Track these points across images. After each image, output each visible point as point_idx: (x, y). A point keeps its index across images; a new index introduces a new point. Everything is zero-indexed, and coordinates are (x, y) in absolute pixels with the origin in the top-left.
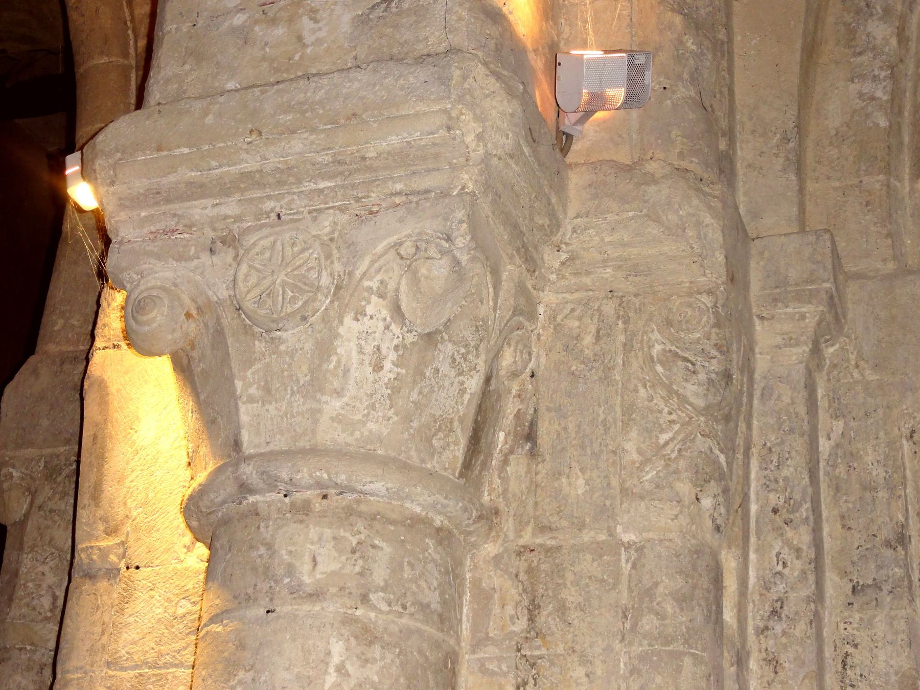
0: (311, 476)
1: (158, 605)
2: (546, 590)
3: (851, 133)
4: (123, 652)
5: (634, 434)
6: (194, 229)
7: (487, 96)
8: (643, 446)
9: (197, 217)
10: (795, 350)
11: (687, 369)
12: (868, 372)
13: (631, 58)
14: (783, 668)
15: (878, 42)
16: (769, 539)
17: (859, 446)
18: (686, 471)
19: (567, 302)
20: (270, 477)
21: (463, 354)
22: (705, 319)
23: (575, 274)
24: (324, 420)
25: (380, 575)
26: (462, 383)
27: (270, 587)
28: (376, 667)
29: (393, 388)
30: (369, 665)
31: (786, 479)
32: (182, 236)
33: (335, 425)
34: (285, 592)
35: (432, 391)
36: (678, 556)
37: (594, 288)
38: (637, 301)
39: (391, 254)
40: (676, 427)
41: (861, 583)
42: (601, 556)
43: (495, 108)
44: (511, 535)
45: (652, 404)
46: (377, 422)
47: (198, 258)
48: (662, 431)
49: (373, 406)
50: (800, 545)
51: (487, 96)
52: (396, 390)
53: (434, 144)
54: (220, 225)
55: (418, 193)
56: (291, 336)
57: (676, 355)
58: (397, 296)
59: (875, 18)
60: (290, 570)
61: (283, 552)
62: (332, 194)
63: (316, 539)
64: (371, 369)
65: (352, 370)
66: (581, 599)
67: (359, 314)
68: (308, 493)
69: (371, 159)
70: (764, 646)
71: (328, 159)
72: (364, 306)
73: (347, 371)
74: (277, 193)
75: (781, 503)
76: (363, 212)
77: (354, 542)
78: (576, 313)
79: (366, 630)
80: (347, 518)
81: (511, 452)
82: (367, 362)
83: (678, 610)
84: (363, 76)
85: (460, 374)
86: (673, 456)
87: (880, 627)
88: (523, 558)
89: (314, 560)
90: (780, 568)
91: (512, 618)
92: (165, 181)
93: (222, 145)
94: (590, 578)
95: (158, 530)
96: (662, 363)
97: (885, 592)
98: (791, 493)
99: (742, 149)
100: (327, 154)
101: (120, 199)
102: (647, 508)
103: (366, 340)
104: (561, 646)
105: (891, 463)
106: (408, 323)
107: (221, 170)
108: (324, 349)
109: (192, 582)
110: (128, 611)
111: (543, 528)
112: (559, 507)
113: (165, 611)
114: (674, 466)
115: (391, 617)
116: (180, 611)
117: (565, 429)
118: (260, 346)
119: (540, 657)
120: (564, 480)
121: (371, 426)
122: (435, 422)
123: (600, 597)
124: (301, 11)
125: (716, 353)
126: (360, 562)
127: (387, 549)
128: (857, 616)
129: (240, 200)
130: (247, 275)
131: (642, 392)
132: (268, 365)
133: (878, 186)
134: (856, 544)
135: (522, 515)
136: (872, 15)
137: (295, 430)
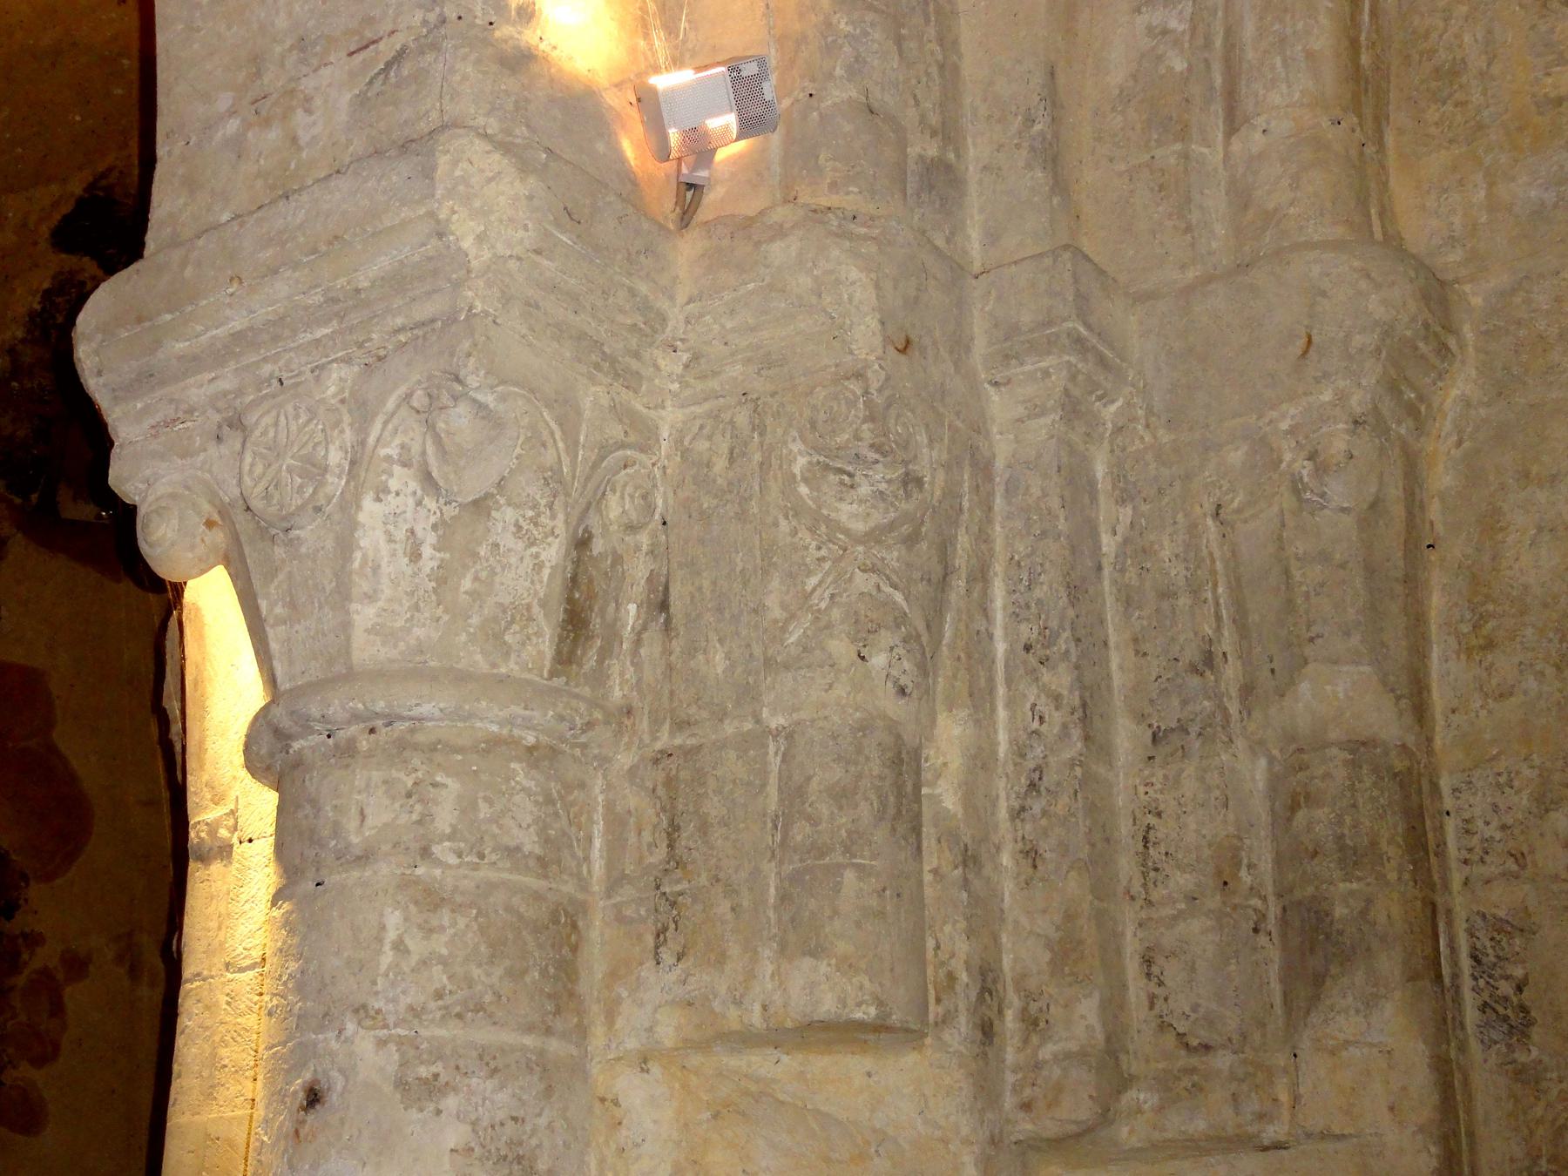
0: (344, 708)
4: (240, 949)
5: (775, 583)
7: (490, 180)
10: (1042, 421)
11: (842, 483)
12: (1161, 432)
14: (1044, 860)
16: (1021, 687)
18: (842, 622)
21: (531, 519)
24: (358, 637)
25: (445, 817)
26: (537, 556)
28: (444, 938)
30: (435, 936)
31: (1039, 602)
35: (493, 573)
36: (834, 738)
39: (404, 412)
43: (503, 193)
45: (796, 540)
46: (424, 625)
48: (809, 573)
49: (417, 608)
51: (490, 180)
53: (430, 259)
54: (220, 404)
56: (308, 532)
57: (827, 467)
60: (337, 830)
64: (406, 560)
65: (384, 564)
67: (381, 492)
70: (1020, 834)
71: (319, 298)
73: (376, 569)
75: (1034, 636)
77: (410, 784)
79: (428, 892)
81: (645, 628)
82: (400, 553)
84: (343, 184)
85: (532, 544)
86: (823, 605)
87: (1189, 786)
90: (1036, 725)
91: (650, 845)
96: (806, 480)
97: (1193, 735)
99: (975, 145)
102: (795, 680)
103: (395, 524)
104: (704, 875)
105: (1192, 554)
107: (209, 334)
108: (346, 546)
111: (681, 725)
115: (462, 871)
117: (700, 589)
118: (279, 552)
119: (681, 894)
120: (701, 657)
122: (504, 612)
124: (294, 103)
125: (877, 456)
126: (418, 807)
127: (453, 785)
128: (1160, 773)
130: (252, 465)
133: (1172, 161)
134: (1154, 675)
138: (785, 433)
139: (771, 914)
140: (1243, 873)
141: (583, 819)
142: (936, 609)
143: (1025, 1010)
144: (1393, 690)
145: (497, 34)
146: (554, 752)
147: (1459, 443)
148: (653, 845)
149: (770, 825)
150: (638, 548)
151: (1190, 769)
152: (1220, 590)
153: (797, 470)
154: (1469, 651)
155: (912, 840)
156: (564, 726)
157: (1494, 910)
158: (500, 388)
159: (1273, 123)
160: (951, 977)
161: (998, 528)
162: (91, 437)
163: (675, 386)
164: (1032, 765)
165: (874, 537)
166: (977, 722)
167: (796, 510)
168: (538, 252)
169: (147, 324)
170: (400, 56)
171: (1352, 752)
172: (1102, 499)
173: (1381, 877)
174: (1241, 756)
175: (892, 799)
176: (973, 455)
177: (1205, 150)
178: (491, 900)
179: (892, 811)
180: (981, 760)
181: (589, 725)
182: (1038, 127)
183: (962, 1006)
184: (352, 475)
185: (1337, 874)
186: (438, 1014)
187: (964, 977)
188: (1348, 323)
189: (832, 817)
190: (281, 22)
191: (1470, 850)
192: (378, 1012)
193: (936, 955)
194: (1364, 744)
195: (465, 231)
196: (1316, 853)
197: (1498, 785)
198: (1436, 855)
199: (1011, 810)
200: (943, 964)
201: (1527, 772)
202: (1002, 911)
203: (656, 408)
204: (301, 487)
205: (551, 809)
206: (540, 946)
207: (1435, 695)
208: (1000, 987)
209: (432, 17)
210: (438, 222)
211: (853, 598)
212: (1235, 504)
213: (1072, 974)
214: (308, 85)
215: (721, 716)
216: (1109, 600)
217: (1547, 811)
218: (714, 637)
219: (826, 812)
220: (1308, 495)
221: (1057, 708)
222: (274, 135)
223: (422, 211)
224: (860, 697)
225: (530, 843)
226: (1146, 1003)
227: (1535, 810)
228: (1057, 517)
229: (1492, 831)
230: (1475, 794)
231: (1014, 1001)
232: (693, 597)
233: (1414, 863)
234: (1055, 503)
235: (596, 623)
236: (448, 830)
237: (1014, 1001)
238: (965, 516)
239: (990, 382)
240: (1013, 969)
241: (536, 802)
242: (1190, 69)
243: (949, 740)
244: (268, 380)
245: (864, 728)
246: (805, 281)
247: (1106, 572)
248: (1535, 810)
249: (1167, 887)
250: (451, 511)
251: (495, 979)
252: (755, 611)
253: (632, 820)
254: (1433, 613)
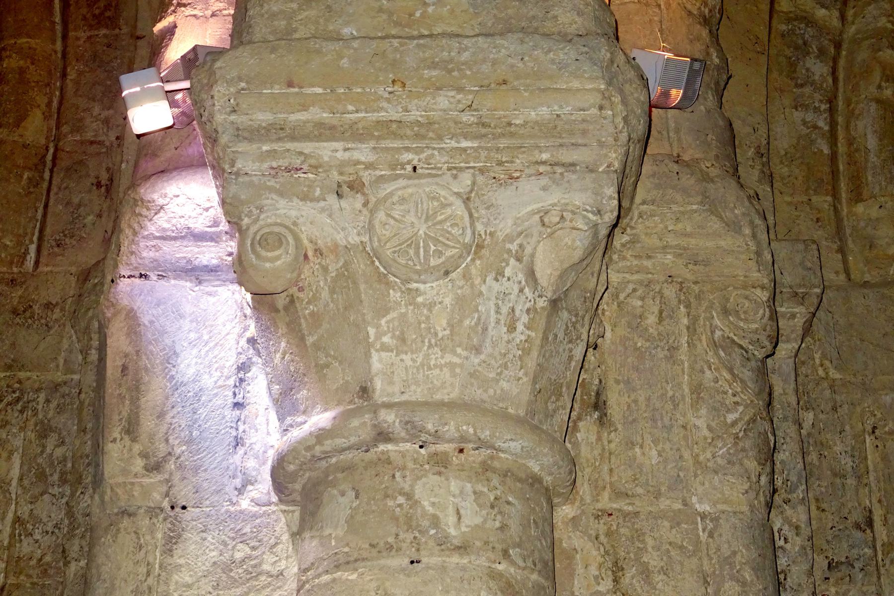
1: (212, 547)
2: (628, 553)
3: (798, 155)
5: (703, 411)
6: (320, 170)
8: (713, 424)
9: (326, 159)
15: (817, 78)
17: (828, 436)
18: (751, 449)
19: (628, 282)
20: (414, 427)
22: (761, 312)
23: (635, 256)
26: (571, 350)
27: (415, 538)
29: (523, 350)
32: (305, 176)
33: (473, 380)
34: (431, 543)
37: (653, 271)
38: (696, 288)
40: (741, 409)
41: (836, 560)
42: (678, 524)
44: (588, 499)
46: (508, 381)
47: (325, 200)
48: (729, 411)
50: (799, 523)
52: (526, 352)
55: (563, 165)
57: (733, 341)
58: (532, 261)
59: (812, 56)
60: (435, 522)
61: (426, 503)
62: (473, 154)
63: (457, 492)
64: (505, 329)
66: (662, 564)
68: (446, 445)
69: (516, 125)
72: (504, 268)
73: (485, 329)
74: (414, 146)
76: (502, 176)
77: (492, 498)
78: (638, 293)
80: (483, 474)
82: (503, 322)
83: (755, 579)
85: (570, 342)
88: (602, 522)
89: (458, 513)
91: (596, 578)
92: (293, 117)
93: (359, 90)
94: (670, 543)
95: (206, 470)
98: (788, 474)
100: (473, 115)
102: (720, 482)
103: (503, 300)
106: (539, 288)
109: (249, 526)
110: (177, 552)
111: (619, 494)
112: (634, 475)
113: (221, 555)
114: (741, 444)
116: (238, 555)
117: (636, 401)
120: (637, 450)
121: (504, 384)
123: (682, 564)
126: (499, 517)
129: (374, 148)
131: (708, 373)
132: (404, 315)
133: (826, 206)
134: (830, 525)
135: (596, 480)
136: (808, 53)
137: (432, 383)
232: (629, 406)
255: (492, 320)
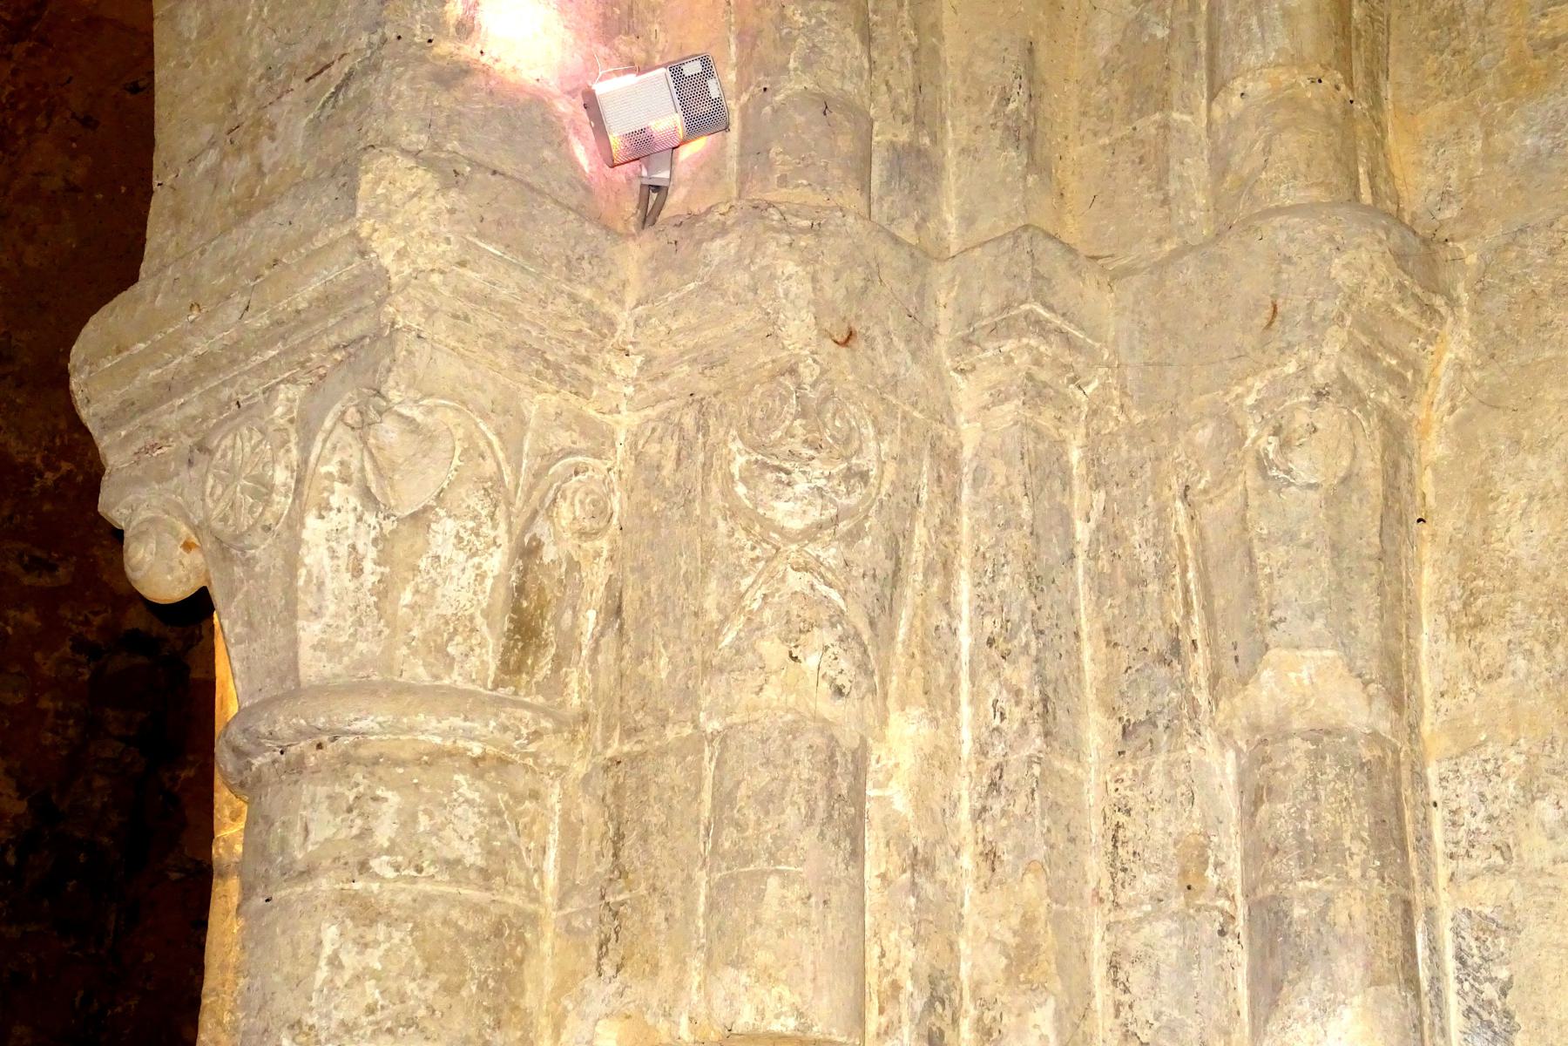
3: (1122, 59)
5: (713, 585)
11: (779, 481)
13: (676, 71)
16: (984, 684)
24: (305, 654)
26: (479, 566)
28: (380, 951)
29: (378, 594)
30: (369, 950)
31: (1002, 593)
33: (318, 653)
35: (435, 585)
36: (763, 742)
38: (716, 402)
39: (340, 429)
42: (684, 758)
45: (733, 540)
48: (745, 573)
49: (360, 623)
53: (356, 277)
54: (191, 429)
57: (765, 465)
64: (349, 576)
65: (327, 581)
67: (324, 509)
70: (980, 835)
75: (997, 630)
77: (351, 798)
78: (657, 434)
81: (602, 634)
82: (343, 568)
85: (473, 555)
86: (755, 606)
87: (1158, 782)
90: (997, 722)
96: (744, 480)
97: (1161, 728)
101: (102, 419)
104: (643, 885)
105: (1161, 539)
108: (292, 563)
111: (630, 732)
115: (401, 885)
119: (622, 903)
121: (361, 646)
122: (447, 623)
125: (812, 452)
126: (359, 822)
127: (394, 798)
128: (1130, 768)
133: (1153, 131)
134: (1125, 666)
138: (727, 433)
139: (701, 924)
140: (1209, 872)
141: (535, 829)
142: (884, 608)
143: (980, 1019)
144: (1360, 676)
145: (436, 50)
146: (503, 762)
147: (1453, 409)
148: (600, 854)
149: (702, 832)
150: (598, 554)
151: (1159, 761)
152: (1191, 575)
153: (735, 469)
154: (1458, 629)
155: (846, 844)
156: (509, 736)
157: (1479, 908)
158: (425, 402)
159: (1250, 85)
160: (896, 987)
161: (965, 519)
162: (83, 468)
163: (630, 390)
164: (992, 763)
165: (811, 533)
166: (934, 721)
167: (733, 513)
168: (462, 264)
169: (126, 354)
170: (349, 77)
171: (1316, 742)
172: (1076, 482)
173: (1343, 876)
174: (1209, 749)
175: (821, 803)
176: (933, 447)
177: (1187, 118)
178: (428, 913)
179: (821, 814)
180: (938, 761)
181: (537, 735)
182: (1012, 106)
183: (905, 1018)
184: (297, 493)
185: (1296, 873)
186: (369, 1030)
187: (908, 986)
188: (1311, 289)
189: (758, 823)
190: (255, 53)
191: (1457, 843)
192: (312, 1027)
193: (881, 964)
194: (1328, 733)
195: (385, 249)
196: (1277, 850)
197: (1484, 771)
198: (1416, 849)
199: (973, 810)
200: (887, 972)
201: (1515, 759)
202: (961, 915)
203: (610, 412)
204: (252, 506)
205: (496, 820)
206: (479, 959)
207: (1425, 679)
208: (955, 996)
209: (376, 38)
210: (360, 240)
211: (785, 598)
212: (1201, 486)
213: (1028, 981)
214: (272, 113)
215: (663, 721)
216: (1083, 590)
217: (1533, 799)
218: (659, 642)
219: (752, 817)
220: (1274, 473)
221: (1017, 703)
222: (244, 164)
223: (346, 231)
224: (792, 699)
225: (473, 856)
226: (1112, 1010)
227: (1522, 800)
228: (1020, 505)
229: (1475, 823)
230: (1462, 783)
231: (970, 1010)
233: (1381, 858)
234: (1018, 490)
235: (549, 630)
236: (386, 844)
237: (970, 1010)
238: (923, 509)
239: (955, 370)
240: (971, 977)
241: (480, 813)
242: (1171, 36)
243: (902, 739)
244: (227, 404)
245: (793, 731)
246: (743, 278)
247: (1081, 559)
248: (1522, 800)
249: (1133, 888)
250: (389, 526)
251: (429, 994)
252: (696, 614)
253: (584, 829)
254: (1424, 591)
255: (328, 569)
